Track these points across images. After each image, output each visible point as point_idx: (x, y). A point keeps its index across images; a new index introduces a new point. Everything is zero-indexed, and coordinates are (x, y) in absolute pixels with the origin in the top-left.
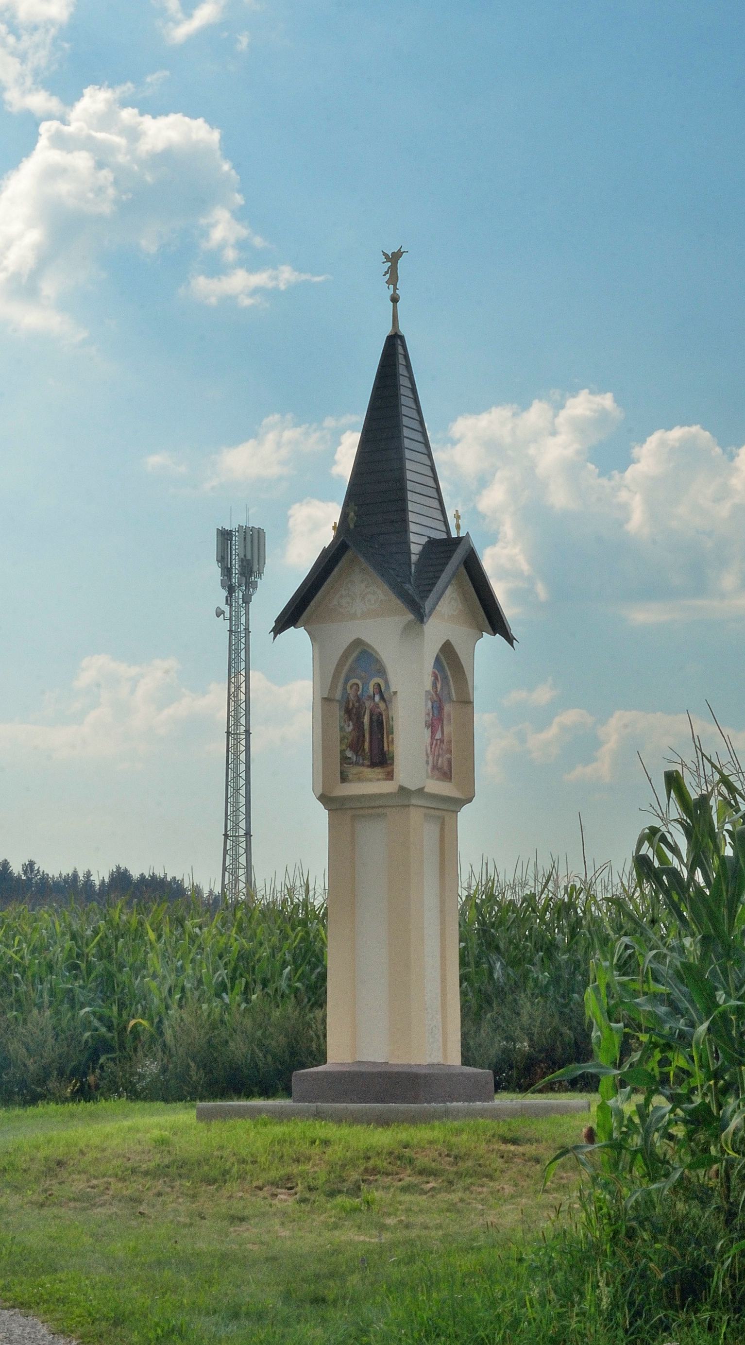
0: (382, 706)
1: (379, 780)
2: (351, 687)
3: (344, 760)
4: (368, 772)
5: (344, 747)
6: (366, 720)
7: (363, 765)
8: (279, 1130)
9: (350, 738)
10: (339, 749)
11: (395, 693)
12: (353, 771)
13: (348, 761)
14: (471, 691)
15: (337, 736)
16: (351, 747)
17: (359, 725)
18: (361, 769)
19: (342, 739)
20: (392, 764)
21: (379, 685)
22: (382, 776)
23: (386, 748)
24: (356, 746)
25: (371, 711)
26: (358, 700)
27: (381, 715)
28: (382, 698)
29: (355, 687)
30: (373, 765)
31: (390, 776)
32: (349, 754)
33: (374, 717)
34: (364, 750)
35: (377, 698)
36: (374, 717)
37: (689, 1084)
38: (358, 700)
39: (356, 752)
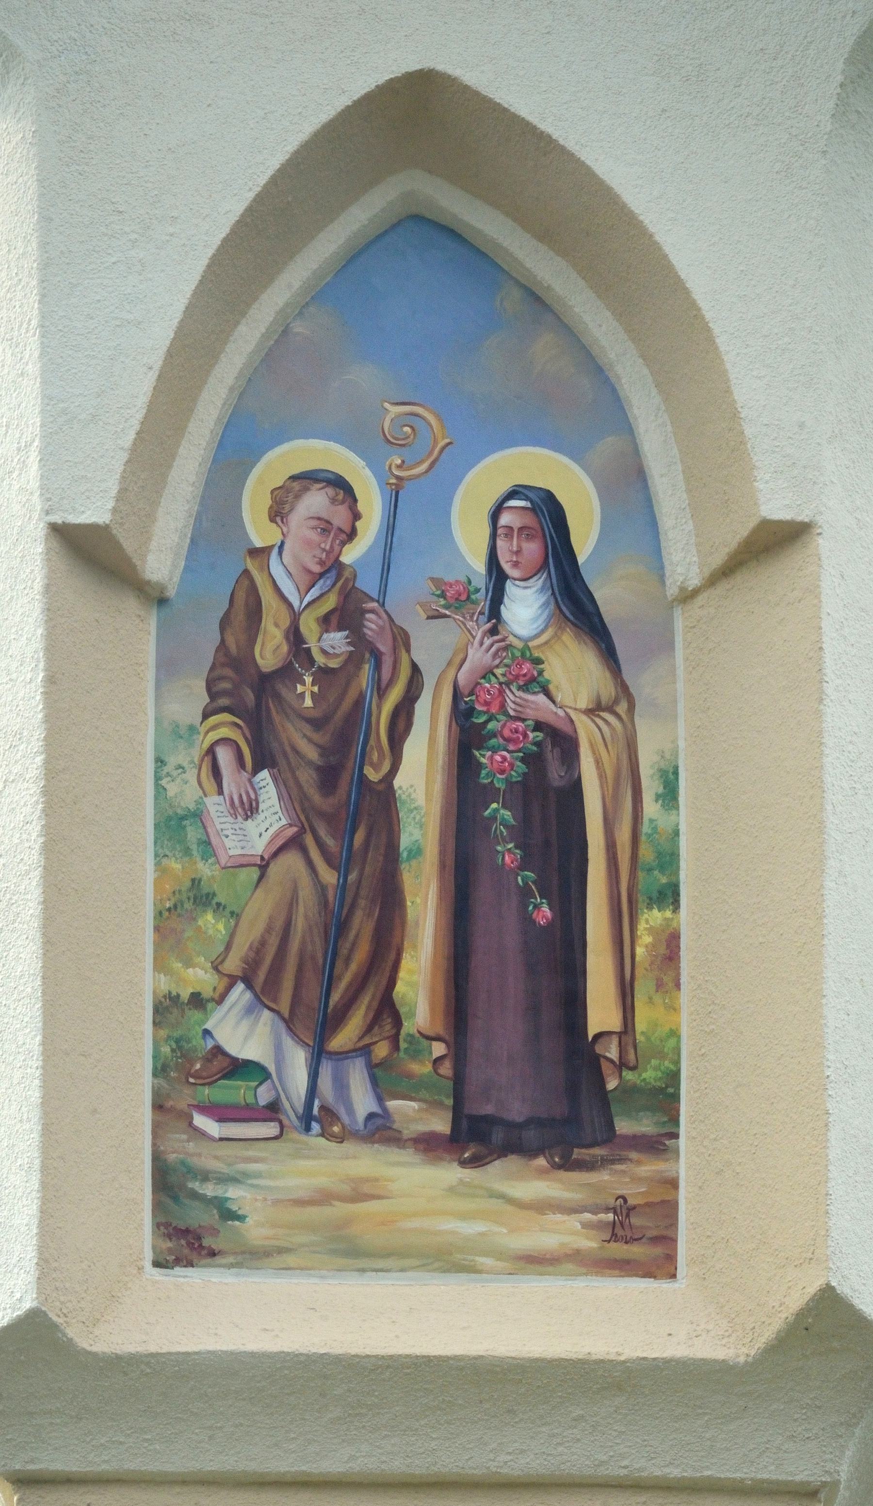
0: (573, 675)
1: (536, 1262)
2: (278, 513)
3: (194, 1077)
4: (422, 1188)
5: (200, 977)
6: (419, 776)
7: (380, 1130)
8: (372, 846)
9: (260, 910)
10: (148, 985)
11: (776, 541)
12: (273, 1178)
13: (236, 1091)
14: (397, 829)
15: (141, 881)
16: (259, 977)
17: (347, 807)
18: (365, 1162)
19: (173, 918)
20: (661, 1144)
21: (549, 513)
22: (568, 1233)
23: (601, 1013)
24: (324, 976)
25: (462, 713)
26: (347, 615)
27: (564, 743)
28: (576, 606)
29: (316, 501)
30: (474, 1137)
31: (640, 1239)
32: (243, 1031)
33: (497, 763)
34: (388, 1010)
35: (526, 609)
36: (497, 763)
37: (611, 1061)
38: (347, 615)
39: (317, 1025)
